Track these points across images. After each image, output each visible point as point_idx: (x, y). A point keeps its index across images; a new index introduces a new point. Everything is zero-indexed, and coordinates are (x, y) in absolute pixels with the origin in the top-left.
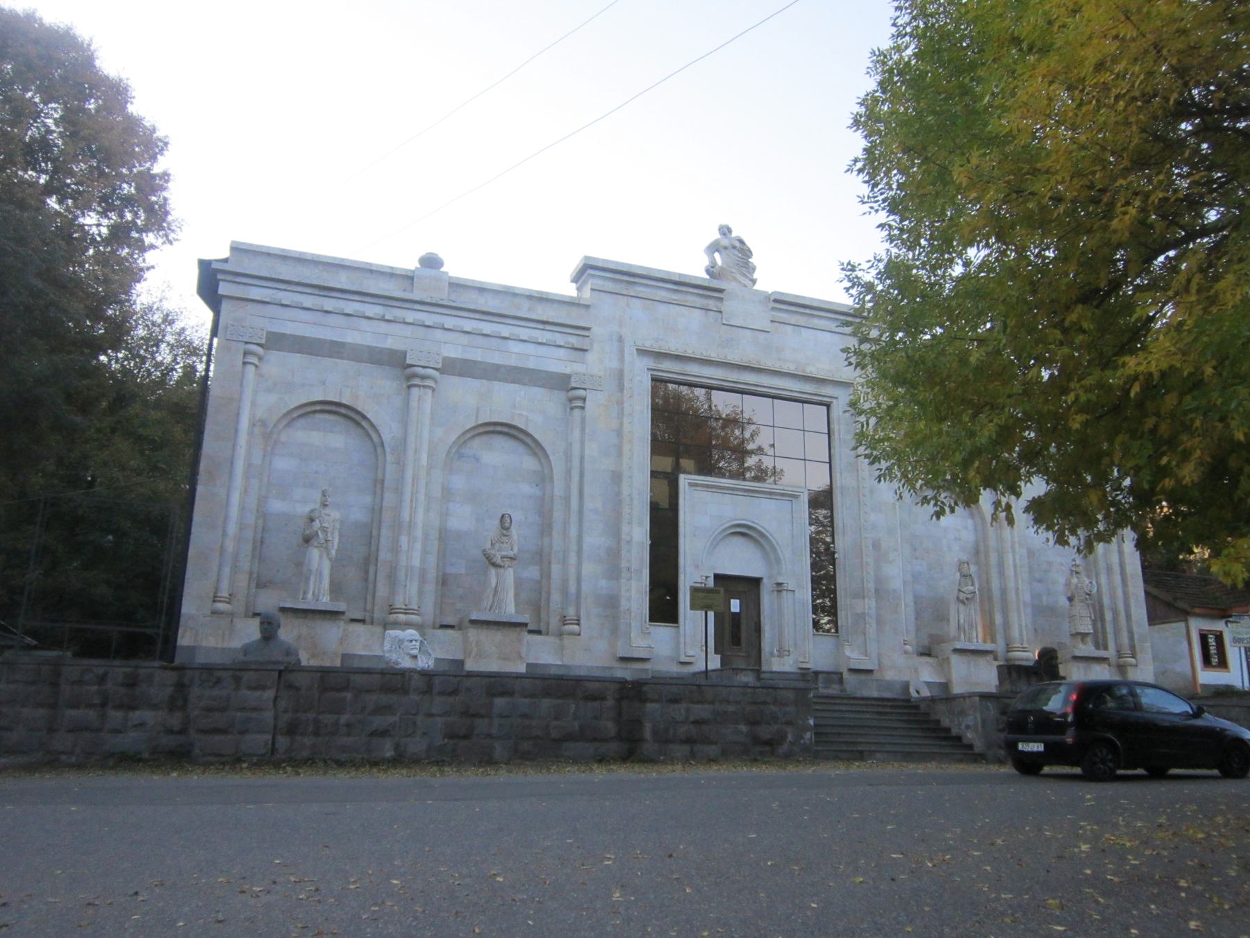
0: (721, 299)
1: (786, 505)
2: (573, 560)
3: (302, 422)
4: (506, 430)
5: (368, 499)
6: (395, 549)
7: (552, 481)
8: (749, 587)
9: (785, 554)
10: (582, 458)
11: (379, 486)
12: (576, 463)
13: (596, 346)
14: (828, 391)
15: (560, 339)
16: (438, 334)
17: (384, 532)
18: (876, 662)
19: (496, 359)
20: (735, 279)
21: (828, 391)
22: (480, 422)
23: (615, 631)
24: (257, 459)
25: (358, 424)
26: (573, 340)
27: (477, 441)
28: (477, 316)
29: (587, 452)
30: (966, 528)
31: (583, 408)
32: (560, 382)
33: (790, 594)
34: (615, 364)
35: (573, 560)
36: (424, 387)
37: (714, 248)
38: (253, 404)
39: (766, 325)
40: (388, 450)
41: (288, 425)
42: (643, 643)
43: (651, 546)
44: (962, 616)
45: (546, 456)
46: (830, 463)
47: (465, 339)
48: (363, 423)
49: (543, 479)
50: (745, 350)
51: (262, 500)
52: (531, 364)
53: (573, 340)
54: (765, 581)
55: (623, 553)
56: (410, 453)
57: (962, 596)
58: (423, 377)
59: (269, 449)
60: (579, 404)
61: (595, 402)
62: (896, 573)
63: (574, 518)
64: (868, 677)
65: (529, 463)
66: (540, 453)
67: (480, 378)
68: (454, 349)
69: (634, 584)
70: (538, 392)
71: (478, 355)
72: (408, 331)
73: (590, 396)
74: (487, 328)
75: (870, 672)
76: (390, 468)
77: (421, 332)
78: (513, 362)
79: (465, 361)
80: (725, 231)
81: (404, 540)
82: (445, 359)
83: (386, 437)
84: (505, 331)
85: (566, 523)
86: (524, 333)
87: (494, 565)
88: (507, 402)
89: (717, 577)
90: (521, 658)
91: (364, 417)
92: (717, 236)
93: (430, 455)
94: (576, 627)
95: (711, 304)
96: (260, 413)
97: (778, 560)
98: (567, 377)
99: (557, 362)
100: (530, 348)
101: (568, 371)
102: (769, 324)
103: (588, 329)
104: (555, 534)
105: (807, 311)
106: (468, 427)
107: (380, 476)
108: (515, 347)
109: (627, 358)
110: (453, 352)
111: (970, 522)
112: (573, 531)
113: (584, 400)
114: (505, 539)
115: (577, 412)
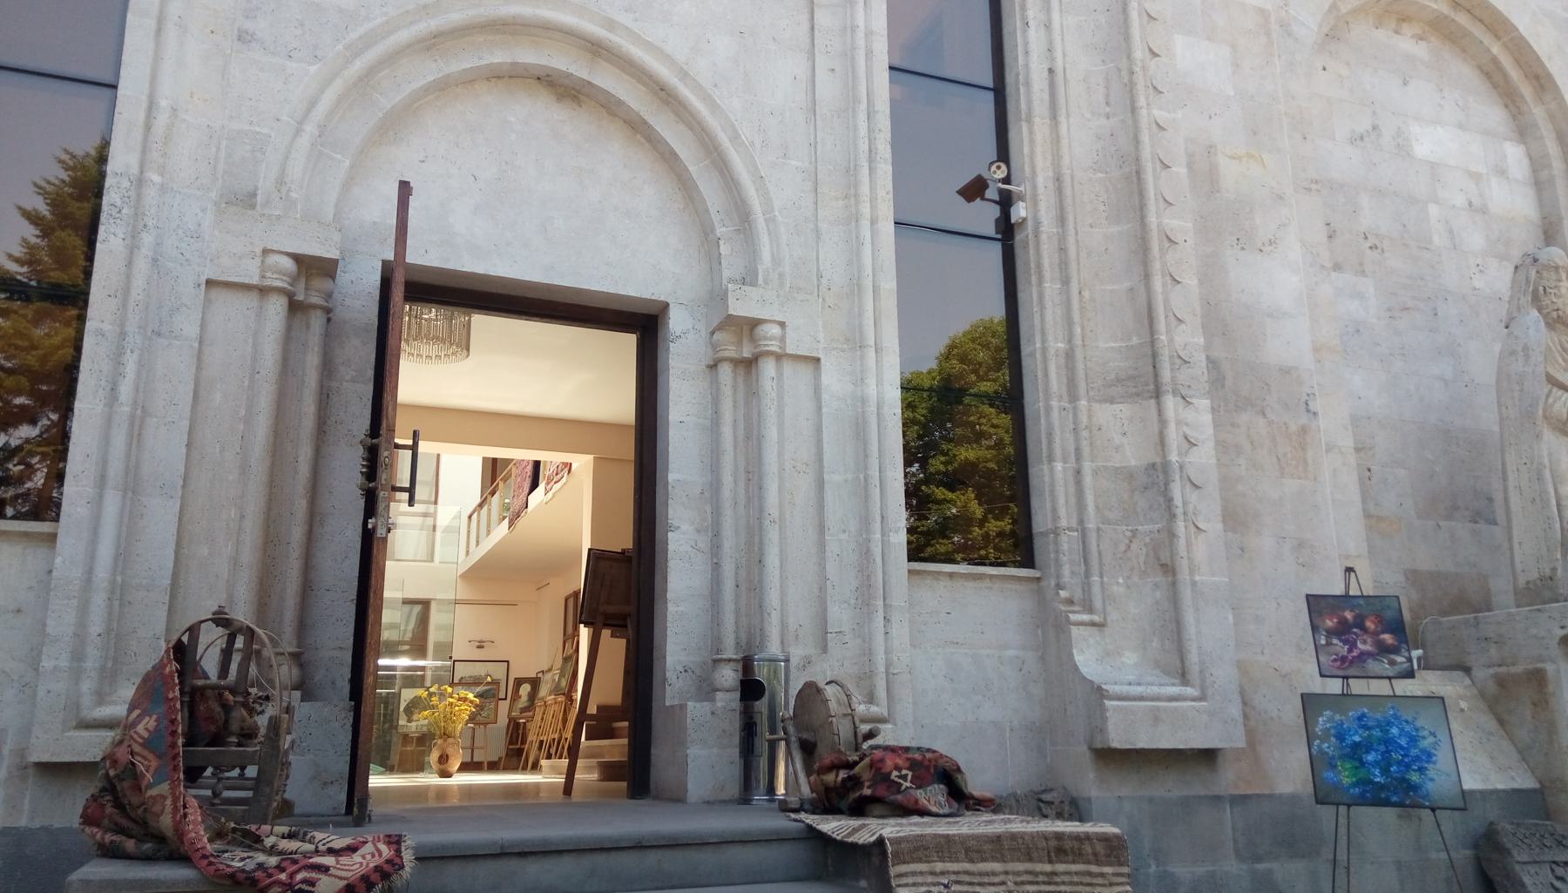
9: (778, 185)
30: (1501, 172)
62: (1286, 290)
64: (1194, 785)
75: (1208, 757)
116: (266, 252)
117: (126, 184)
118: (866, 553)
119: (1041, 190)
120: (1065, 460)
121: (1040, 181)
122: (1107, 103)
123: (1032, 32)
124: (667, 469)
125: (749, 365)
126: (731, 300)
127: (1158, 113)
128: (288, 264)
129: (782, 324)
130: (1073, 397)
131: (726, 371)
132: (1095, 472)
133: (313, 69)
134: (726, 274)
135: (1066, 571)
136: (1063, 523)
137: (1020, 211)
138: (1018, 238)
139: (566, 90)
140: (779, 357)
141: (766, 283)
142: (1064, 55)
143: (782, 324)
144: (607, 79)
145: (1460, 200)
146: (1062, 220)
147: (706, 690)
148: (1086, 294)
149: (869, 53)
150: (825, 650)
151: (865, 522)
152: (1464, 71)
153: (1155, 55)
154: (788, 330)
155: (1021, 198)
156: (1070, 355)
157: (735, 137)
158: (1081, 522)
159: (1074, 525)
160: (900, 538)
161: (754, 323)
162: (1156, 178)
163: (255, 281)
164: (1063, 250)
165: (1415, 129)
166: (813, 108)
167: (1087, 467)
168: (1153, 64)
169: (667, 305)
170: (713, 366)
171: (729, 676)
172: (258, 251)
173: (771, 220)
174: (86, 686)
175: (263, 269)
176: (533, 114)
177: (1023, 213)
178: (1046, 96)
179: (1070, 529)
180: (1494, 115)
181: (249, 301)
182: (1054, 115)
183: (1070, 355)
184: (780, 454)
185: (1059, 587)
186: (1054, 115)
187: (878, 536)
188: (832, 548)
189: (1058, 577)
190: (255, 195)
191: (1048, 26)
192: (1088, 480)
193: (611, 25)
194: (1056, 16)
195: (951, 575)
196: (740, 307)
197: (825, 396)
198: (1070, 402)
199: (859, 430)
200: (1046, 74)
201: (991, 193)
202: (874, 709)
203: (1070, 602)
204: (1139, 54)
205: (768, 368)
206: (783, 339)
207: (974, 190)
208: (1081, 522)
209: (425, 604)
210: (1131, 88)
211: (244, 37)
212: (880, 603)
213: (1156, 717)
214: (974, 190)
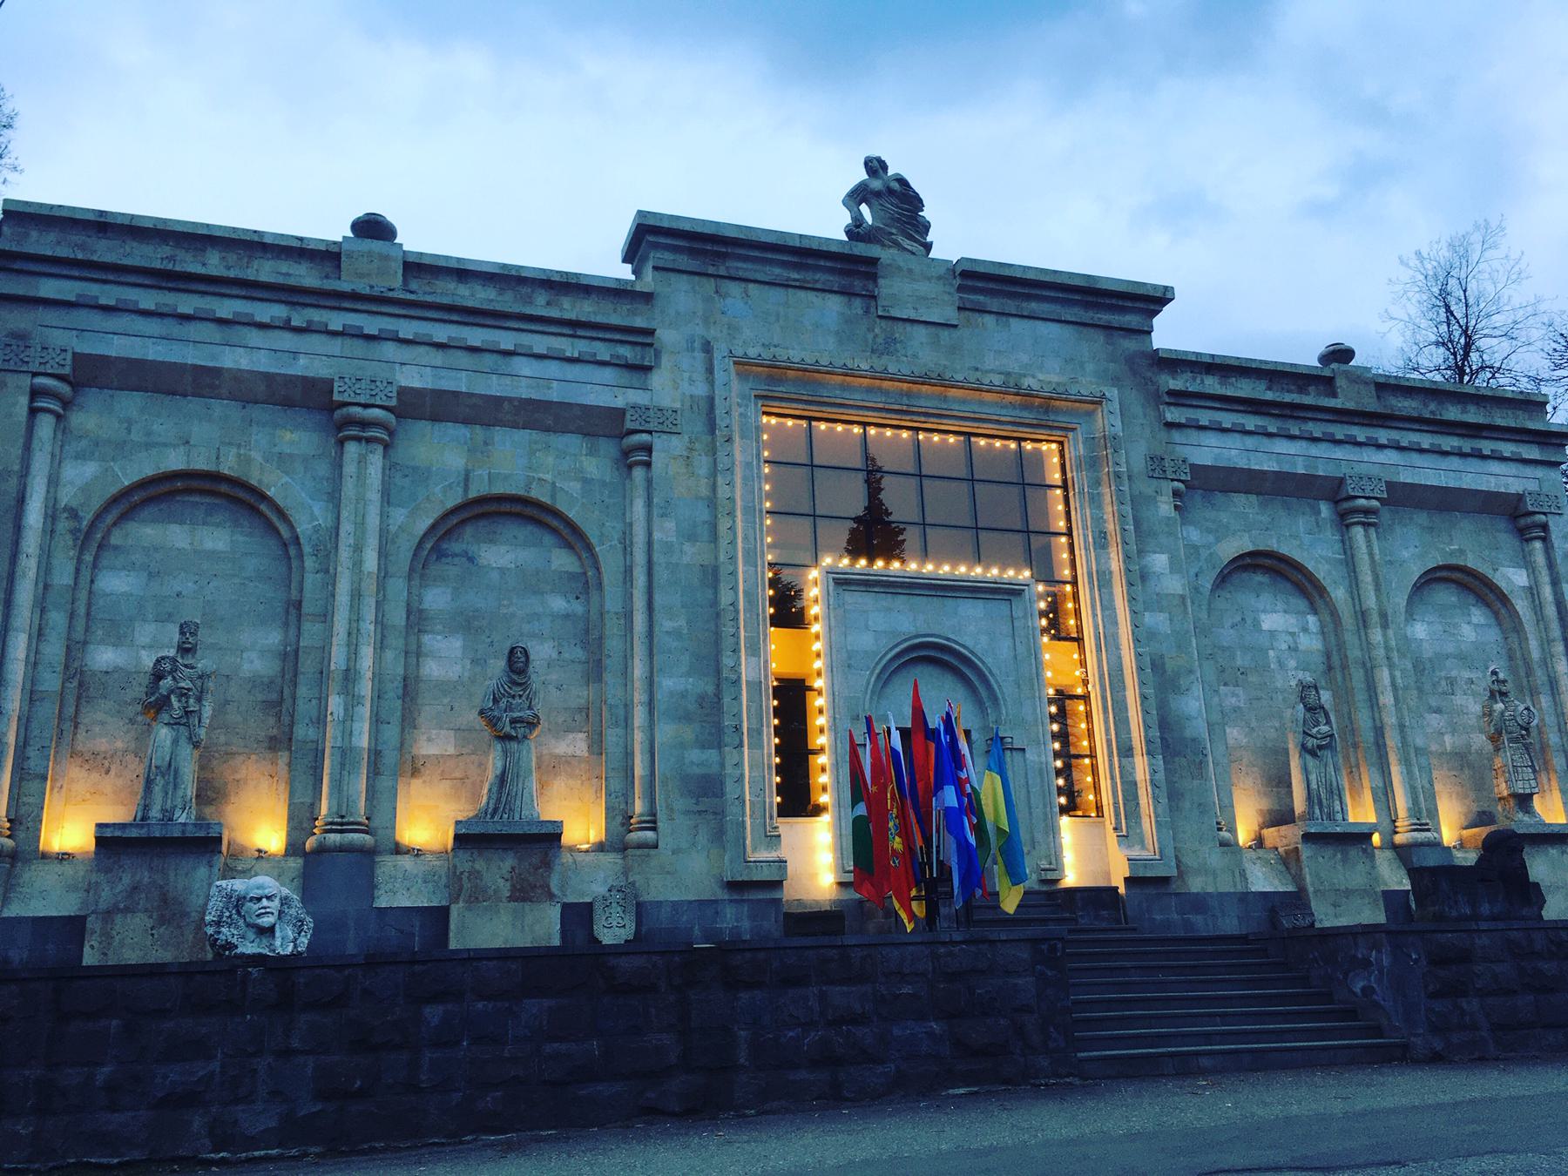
0: (873, 277)
1: (1004, 606)
2: (639, 716)
3: (150, 511)
4: (517, 508)
5: (273, 638)
6: (320, 721)
7: (600, 586)
10: (650, 544)
11: (293, 611)
12: (640, 557)
15: (603, 351)
16: (389, 350)
17: (302, 691)
18: (1173, 863)
19: (495, 387)
20: (897, 245)
22: (472, 494)
24: (63, 575)
25: (254, 510)
26: (626, 352)
27: (469, 530)
28: (455, 318)
29: (657, 535)
30: (1305, 630)
31: (648, 465)
32: (605, 425)
34: (701, 390)
35: (639, 716)
36: (369, 440)
37: (858, 195)
38: (53, 481)
39: (951, 315)
40: (307, 549)
41: (124, 517)
44: (1313, 777)
45: (589, 547)
47: (437, 357)
48: (263, 507)
49: (586, 584)
51: (75, 648)
52: (555, 394)
53: (626, 352)
55: (726, 700)
56: (344, 554)
57: (1311, 742)
58: (364, 424)
59: (88, 558)
61: (667, 452)
63: (639, 649)
65: (562, 561)
66: (579, 546)
67: (466, 422)
68: (417, 372)
70: (572, 443)
71: (460, 383)
72: (336, 346)
73: (658, 442)
74: (475, 336)
75: (1165, 880)
76: (311, 580)
77: (358, 347)
78: (524, 391)
79: (439, 394)
80: (875, 166)
81: (335, 704)
82: (403, 392)
83: (303, 527)
84: (506, 340)
85: (627, 658)
86: (540, 343)
87: (507, 738)
88: (512, 462)
90: (551, 896)
91: (263, 497)
92: (863, 175)
93: (383, 554)
94: (650, 834)
95: (858, 285)
96: (66, 496)
98: (620, 413)
99: (599, 389)
100: (553, 369)
101: (619, 403)
103: (650, 332)
104: (607, 677)
106: (450, 504)
107: (294, 594)
108: (525, 367)
109: (719, 375)
110: (412, 379)
111: (1311, 619)
112: (639, 670)
113: (648, 449)
114: (517, 690)
115: (639, 473)
145: (1284, 646)
152: (1289, 585)
165: (1263, 616)
180: (1302, 604)
193: (948, 639)
213: (1145, 866)
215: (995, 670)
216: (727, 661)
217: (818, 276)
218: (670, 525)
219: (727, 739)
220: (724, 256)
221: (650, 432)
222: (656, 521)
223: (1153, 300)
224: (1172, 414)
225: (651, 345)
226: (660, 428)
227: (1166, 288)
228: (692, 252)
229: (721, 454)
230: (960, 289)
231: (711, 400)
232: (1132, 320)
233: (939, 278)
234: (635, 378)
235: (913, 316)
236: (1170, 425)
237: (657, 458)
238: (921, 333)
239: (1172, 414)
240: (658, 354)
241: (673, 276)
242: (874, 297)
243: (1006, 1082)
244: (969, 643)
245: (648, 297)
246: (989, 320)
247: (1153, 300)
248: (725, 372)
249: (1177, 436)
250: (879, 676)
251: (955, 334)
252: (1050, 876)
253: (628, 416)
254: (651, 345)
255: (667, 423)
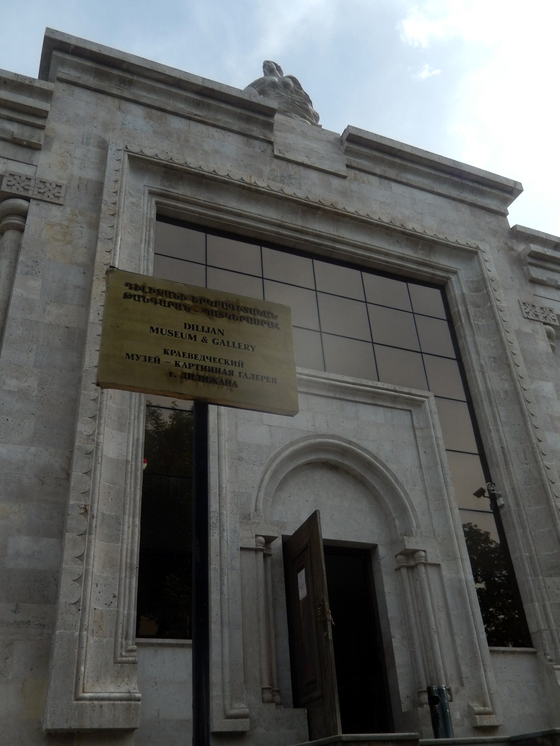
1: (402, 418)
8: (352, 565)
13: (56, 146)
14: (443, 261)
21: (443, 261)
23: (43, 658)
31: (21, 230)
33: (433, 573)
34: (91, 174)
39: (343, 170)
42: (112, 689)
43: (146, 473)
46: (459, 359)
50: (311, 188)
54: (382, 551)
55: (76, 473)
60: (15, 220)
69: (98, 548)
73: (33, 208)
89: (56, 47)
92: (260, 74)
95: (256, 131)
97: (403, 511)
102: (345, 168)
103: (42, 115)
105: (387, 157)
109: (111, 164)
113: (24, 215)
116: (257, 536)
117: (216, 515)
118: (472, 643)
119: (508, 493)
120: (538, 602)
121: (507, 489)
122: (526, 459)
123: (493, 434)
124: (386, 612)
125: (411, 568)
126: (406, 543)
127: (547, 463)
128: (262, 539)
129: (425, 551)
130: (536, 576)
131: (404, 571)
132: (551, 606)
133: (262, 468)
134: (399, 532)
135: (548, 648)
136: (543, 627)
137: (501, 501)
138: (502, 512)
139: (333, 467)
140: (425, 565)
141: (416, 534)
142: (506, 442)
143: (425, 551)
144: (347, 462)
146: (517, 504)
147: (417, 704)
148: (533, 533)
149: (438, 445)
150: (462, 685)
151: (470, 630)
153: (540, 441)
154: (428, 553)
155: (500, 496)
156: (531, 558)
157: (396, 480)
158: (549, 627)
159: (547, 628)
160: (484, 636)
161: (415, 552)
162: (551, 488)
163: (254, 547)
164: (520, 516)
166: (421, 467)
167: (548, 604)
168: (540, 444)
169: (377, 545)
170: (398, 569)
171: (425, 698)
172: (254, 536)
173: (414, 511)
174: (227, 702)
175: (256, 542)
176: (323, 478)
177: (502, 502)
178: (502, 457)
179: (546, 630)
181: (253, 554)
182: (507, 464)
183: (531, 558)
184: (432, 604)
185: (545, 655)
186: (507, 464)
187: (475, 636)
188: (458, 642)
189: (544, 650)
190: (250, 515)
191: (498, 431)
192: (549, 609)
193: (350, 442)
194: (500, 428)
195: (504, 652)
196: (411, 544)
197: (445, 580)
198: (535, 577)
199: (461, 592)
200: (501, 449)
201: (487, 494)
202: (487, 709)
203: (551, 660)
204: (535, 441)
205: (422, 569)
206: (426, 557)
207: (480, 493)
208: (549, 627)
209: (263, 689)
210: (534, 453)
211: (240, 459)
212: (481, 664)
214: (480, 493)
215: (399, 477)
216: (83, 427)
217: (219, 117)
218: (35, 284)
219: (71, 523)
220: (130, 83)
221: (28, 199)
222: (19, 278)
223: (509, 190)
224: (536, 273)
225: (42, 128)
226: (39, 197)
227: (516, 183)
228: (98, 74)
229: (103, 226)
230: (348, 152)
231: (100, 186)
232: (493, 204)
233: (329, 142)
234: (22, 154)
235: (307, 161)
236: (534, 282)
237: (32, 223)
238: (314, 176)
239: (536, 273)
240: (49, 140)
241: (77, 90)
242: (271, 143)
243: (97, 448)
244: (371, 447)
245: (47, 95)
246: (374, 180)
247: (509, 190)
248: (116, 162)
249: (541, 291)
250: (275, 473)
251: (345, 183)
252: (486, 721)
253: (5, 181)
254: (42, 128)
255: (51, 195)
